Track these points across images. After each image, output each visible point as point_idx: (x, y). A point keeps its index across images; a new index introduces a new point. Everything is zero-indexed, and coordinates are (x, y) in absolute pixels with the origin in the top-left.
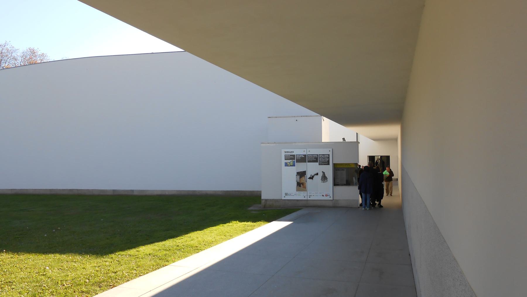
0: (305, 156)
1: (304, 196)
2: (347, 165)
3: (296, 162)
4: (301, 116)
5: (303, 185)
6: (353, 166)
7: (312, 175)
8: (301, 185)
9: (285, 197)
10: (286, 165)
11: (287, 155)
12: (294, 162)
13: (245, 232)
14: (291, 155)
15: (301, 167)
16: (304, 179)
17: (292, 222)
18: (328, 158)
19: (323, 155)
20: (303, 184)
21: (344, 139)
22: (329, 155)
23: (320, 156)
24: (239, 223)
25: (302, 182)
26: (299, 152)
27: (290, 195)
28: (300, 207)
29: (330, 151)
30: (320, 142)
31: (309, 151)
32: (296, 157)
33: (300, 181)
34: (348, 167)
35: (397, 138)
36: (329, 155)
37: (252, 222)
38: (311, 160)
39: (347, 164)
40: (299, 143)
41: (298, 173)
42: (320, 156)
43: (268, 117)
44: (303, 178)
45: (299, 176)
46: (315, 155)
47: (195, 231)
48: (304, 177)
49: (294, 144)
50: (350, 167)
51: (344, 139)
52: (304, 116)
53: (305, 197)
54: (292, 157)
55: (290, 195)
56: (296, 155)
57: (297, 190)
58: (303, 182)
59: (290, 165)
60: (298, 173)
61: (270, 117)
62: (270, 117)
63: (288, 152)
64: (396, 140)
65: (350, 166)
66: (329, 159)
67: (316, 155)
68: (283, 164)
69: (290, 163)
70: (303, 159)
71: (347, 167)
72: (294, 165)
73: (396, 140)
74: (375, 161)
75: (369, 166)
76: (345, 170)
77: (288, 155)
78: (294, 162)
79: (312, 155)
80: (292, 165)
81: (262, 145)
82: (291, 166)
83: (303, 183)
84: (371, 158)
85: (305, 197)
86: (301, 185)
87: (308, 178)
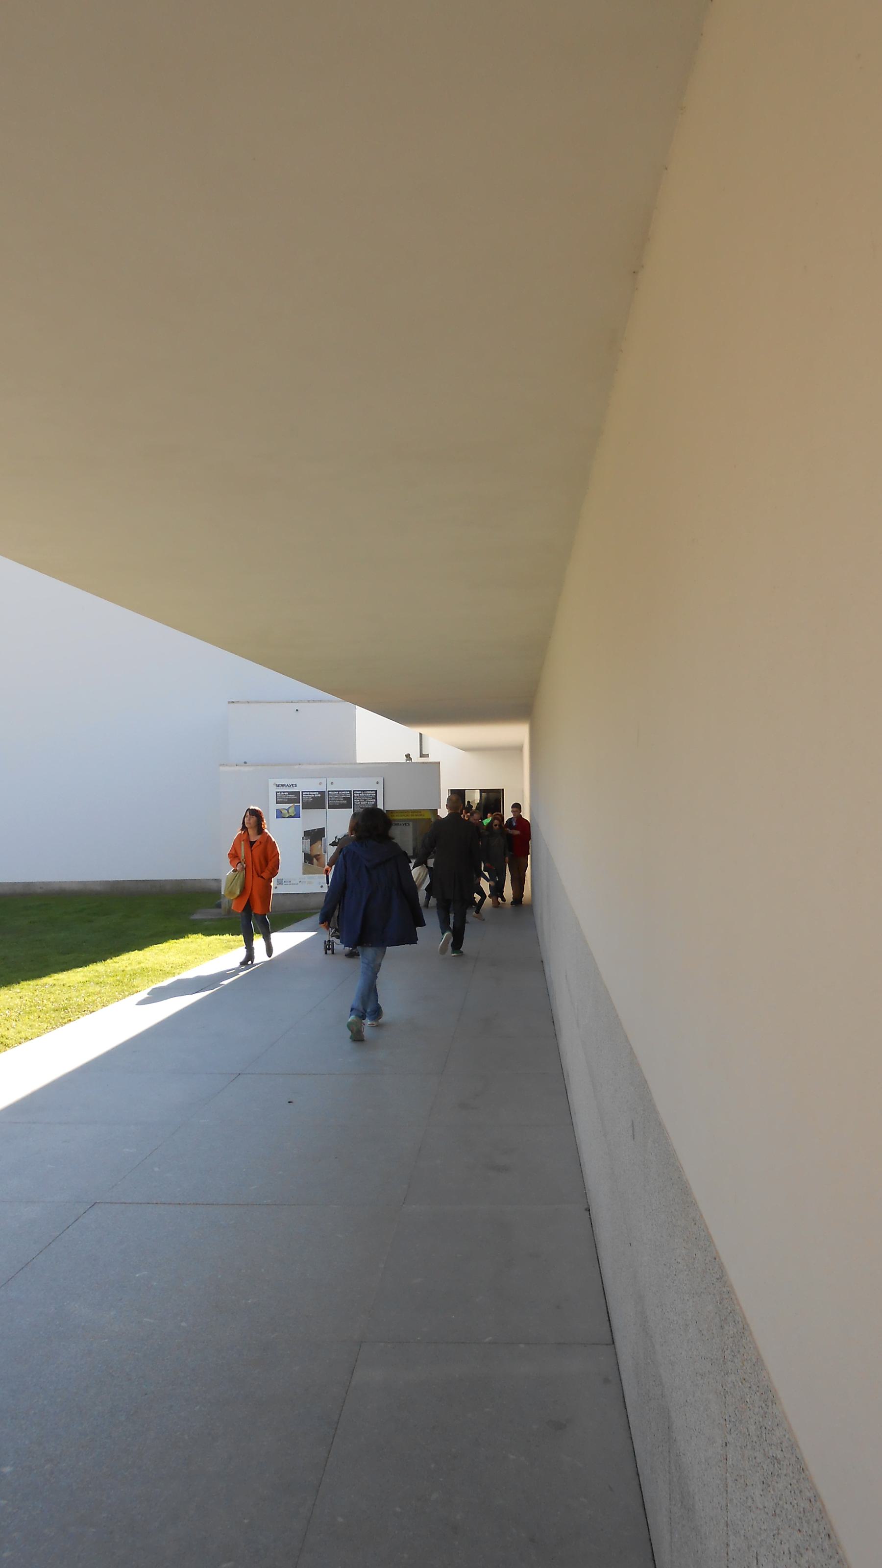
0: (322, 793)
1: (62, 986)
2: (415, 814)
3: (302, 809)
4: (309, 701)
5: (317, 860)
6: (427, 816)
7: (338, 837)
8: (315, 860)
9: (276, 888)
10: (280, 814)
11: (281, 792)
12: (297, 808)
13: (230, 950)
14: (290, 793)
15: (313, 819)
16: (320, 846)
17: (316, 933)
18: (373, 799)
19: (363, 791)
20: (317, 857)
21: (408, 756)
22: (376, 791)
23: (355, 795)
24: (204, 938)
25: (315, 852)
26: (308, 785)
27: (289, 882)
28: (312, 909)
29: (377, 783)
30: (351, 764)
31: (332, 783)
32: (302, 796)
33: (310, 851)
34: (418, 817)
35: (523, 747)
36: (376, 791)
37: (232, 935)
38: (337, 802)
39: (402, 812)
40: (310, 764)
41: (307, 834)
42: (355, 795)
43: (229, 702)
44: (318, 845)
45: (309, 841)
46: (334, 793)
47: (169, 940)
48: (319, 842)
49: (297, 767)
50: (421, 817)
51: (408, 756)
52: (314, 701)
53: (322, 887)
54: (293, 796)
55: (289, 882)
56: (302, 792)
57: (305, 872)
58: (318, 854)
59: (288, 816)
60: (307, 834)
61: (233, 702)
62: (233, 702)
63: (284, 785)
64: (520, 749)
65: (421, 815)
66: (377, 800)
67: (347, 792)
68: (273, 814)
69: (288, 810)
70: (318, 802)
71: (415, 817)
72: (297, 816)
73: (520, 749)
74: (466, 803)
75: (453, 812)
76: (411, 824)
77: (284, 792)
78: (297, 808)
79: (339, 791)
80: (293, 815)
81: (222, 768)
82: (290, 817)
83: (319, 855)
84: (458, 795)
85: (322, 887)
86: (315, 860)
87: (330, 845)
